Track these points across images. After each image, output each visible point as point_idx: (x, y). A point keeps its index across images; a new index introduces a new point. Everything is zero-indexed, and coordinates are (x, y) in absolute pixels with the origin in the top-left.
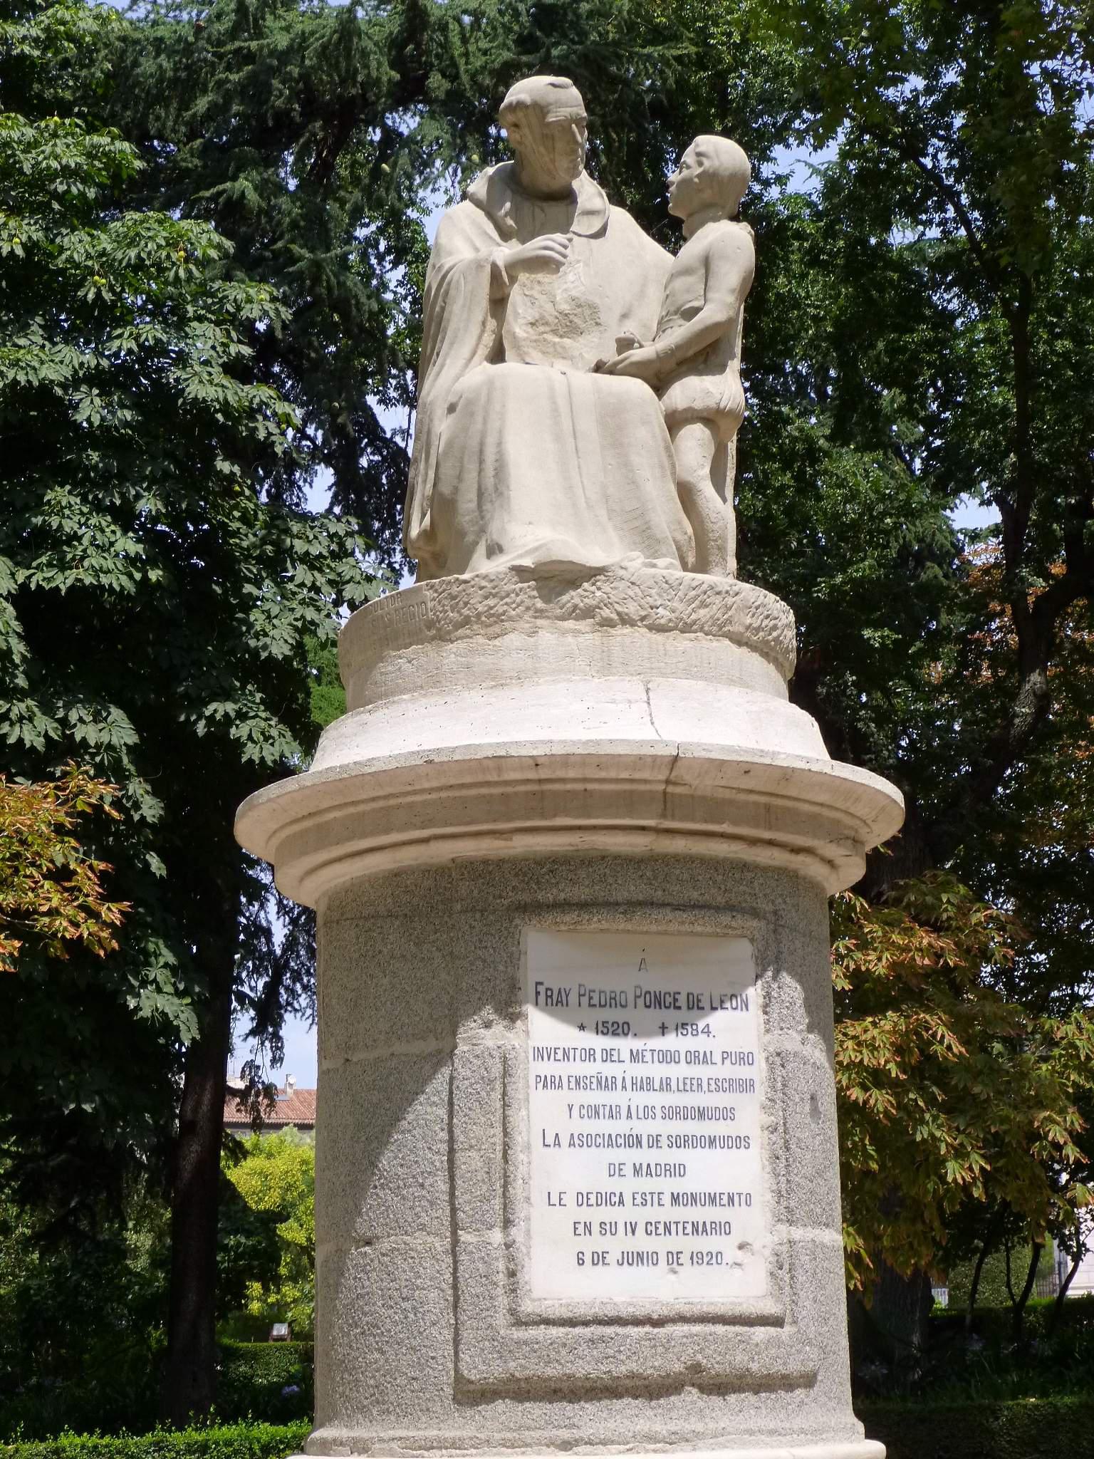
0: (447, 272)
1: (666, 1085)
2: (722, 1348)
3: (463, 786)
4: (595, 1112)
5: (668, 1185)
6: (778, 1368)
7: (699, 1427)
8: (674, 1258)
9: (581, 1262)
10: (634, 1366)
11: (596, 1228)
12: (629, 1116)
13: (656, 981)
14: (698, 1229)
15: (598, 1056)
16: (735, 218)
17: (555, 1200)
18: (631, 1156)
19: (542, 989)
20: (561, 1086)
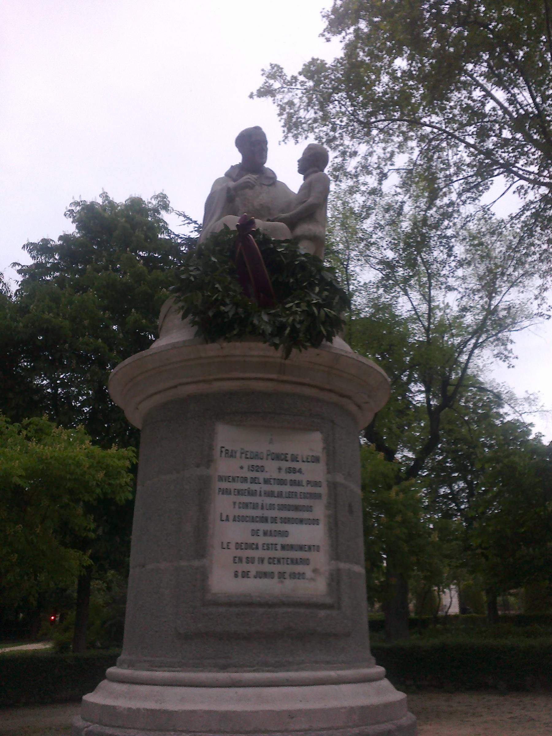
1: (280, 495)
4: (246, 506)
5: (280, 540)
9: (236, 576)
11: (244, 560)
13: (277, 448)
14: (294, 562)
15: (249, 480)
17: (225, 546)
19: (223, 450)
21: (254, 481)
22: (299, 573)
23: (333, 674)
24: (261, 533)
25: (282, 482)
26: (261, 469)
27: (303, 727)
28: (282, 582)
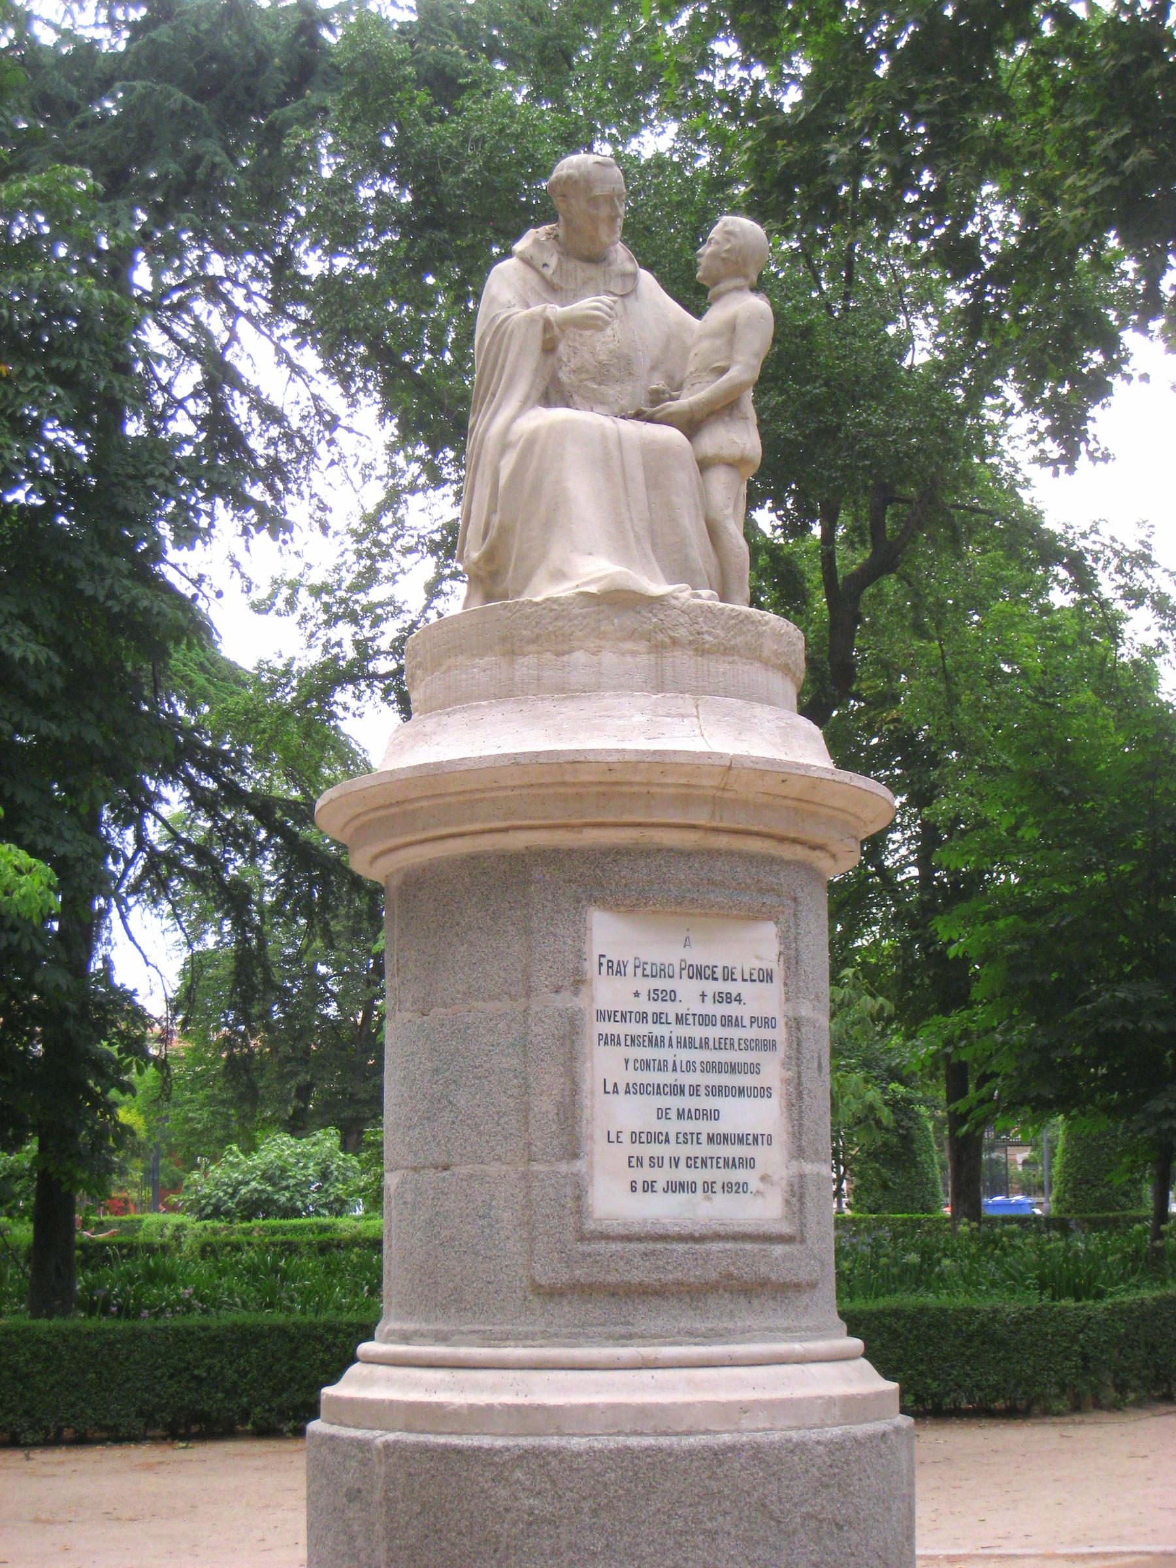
0: (499, 326)
1: (704, 1044)
2: (749, 1261)
3: (542, 785)
4: (646, 1065)
5: (705, 1127)
6: (791, 1278)
7: (731, 1325)
8: (709, 1187)
9: (633, 1189)
10: (679, 1275)
11: (646, 1162)
12: (675, 1070)
13: (698, 956)
14: (731, 1163)
15: (650, 1018)
16: (755, 289)
17: (613, 1137)
18: (675, 1103)
19: (604, 960)
20: (619, 1043)
21: (658, 1018)
22: (737, 1183)
23: (797, 1347)
24: (673, 1114)
25: (706, 1020)
26: (671, 996)
27: (761, 1425)
28: (709, 1199)
